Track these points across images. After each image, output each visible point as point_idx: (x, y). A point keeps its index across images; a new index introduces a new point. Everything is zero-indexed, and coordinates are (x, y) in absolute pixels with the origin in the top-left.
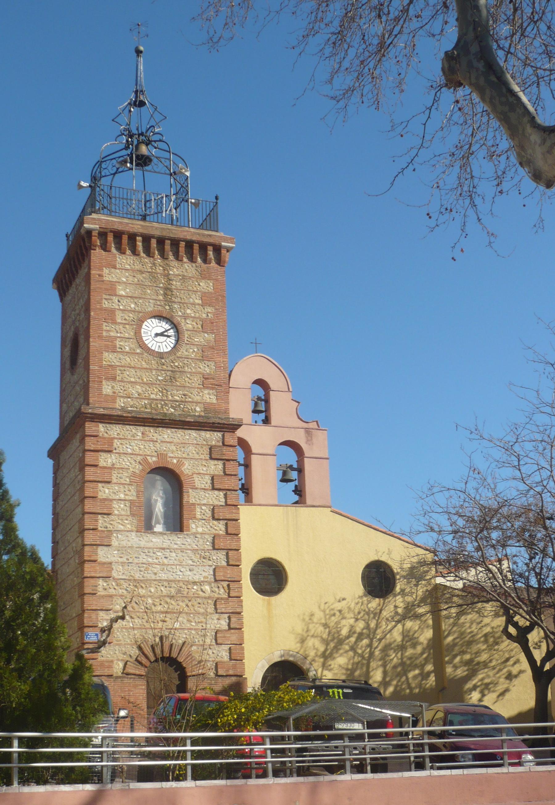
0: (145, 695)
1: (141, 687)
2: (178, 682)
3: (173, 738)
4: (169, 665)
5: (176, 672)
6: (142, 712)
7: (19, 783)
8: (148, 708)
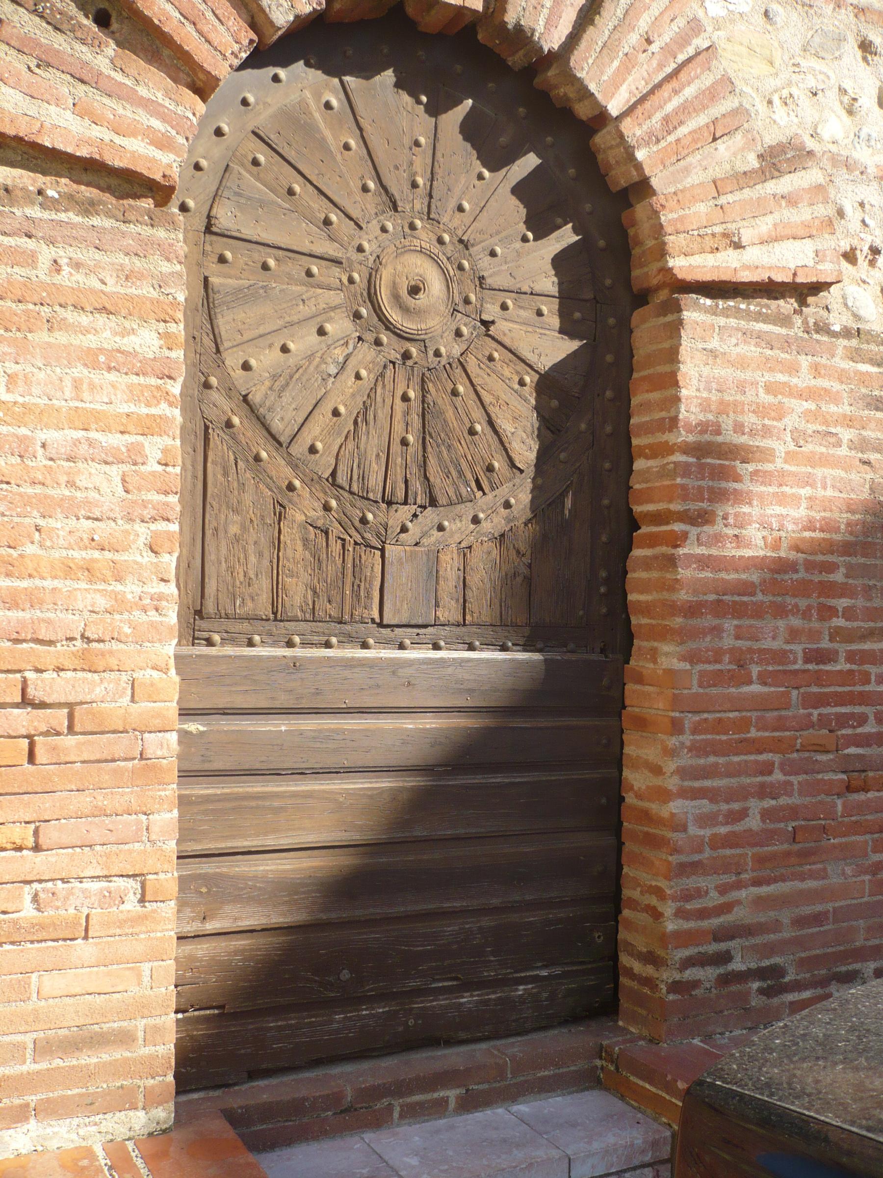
0: (163, 450)
1: (104, 333)
2: (552, 348)
3: (417, 1103)
4: (471, 130)
5: (540, 225)
6: (102, 692)
7: (89, 1153)
8: (197, 620)
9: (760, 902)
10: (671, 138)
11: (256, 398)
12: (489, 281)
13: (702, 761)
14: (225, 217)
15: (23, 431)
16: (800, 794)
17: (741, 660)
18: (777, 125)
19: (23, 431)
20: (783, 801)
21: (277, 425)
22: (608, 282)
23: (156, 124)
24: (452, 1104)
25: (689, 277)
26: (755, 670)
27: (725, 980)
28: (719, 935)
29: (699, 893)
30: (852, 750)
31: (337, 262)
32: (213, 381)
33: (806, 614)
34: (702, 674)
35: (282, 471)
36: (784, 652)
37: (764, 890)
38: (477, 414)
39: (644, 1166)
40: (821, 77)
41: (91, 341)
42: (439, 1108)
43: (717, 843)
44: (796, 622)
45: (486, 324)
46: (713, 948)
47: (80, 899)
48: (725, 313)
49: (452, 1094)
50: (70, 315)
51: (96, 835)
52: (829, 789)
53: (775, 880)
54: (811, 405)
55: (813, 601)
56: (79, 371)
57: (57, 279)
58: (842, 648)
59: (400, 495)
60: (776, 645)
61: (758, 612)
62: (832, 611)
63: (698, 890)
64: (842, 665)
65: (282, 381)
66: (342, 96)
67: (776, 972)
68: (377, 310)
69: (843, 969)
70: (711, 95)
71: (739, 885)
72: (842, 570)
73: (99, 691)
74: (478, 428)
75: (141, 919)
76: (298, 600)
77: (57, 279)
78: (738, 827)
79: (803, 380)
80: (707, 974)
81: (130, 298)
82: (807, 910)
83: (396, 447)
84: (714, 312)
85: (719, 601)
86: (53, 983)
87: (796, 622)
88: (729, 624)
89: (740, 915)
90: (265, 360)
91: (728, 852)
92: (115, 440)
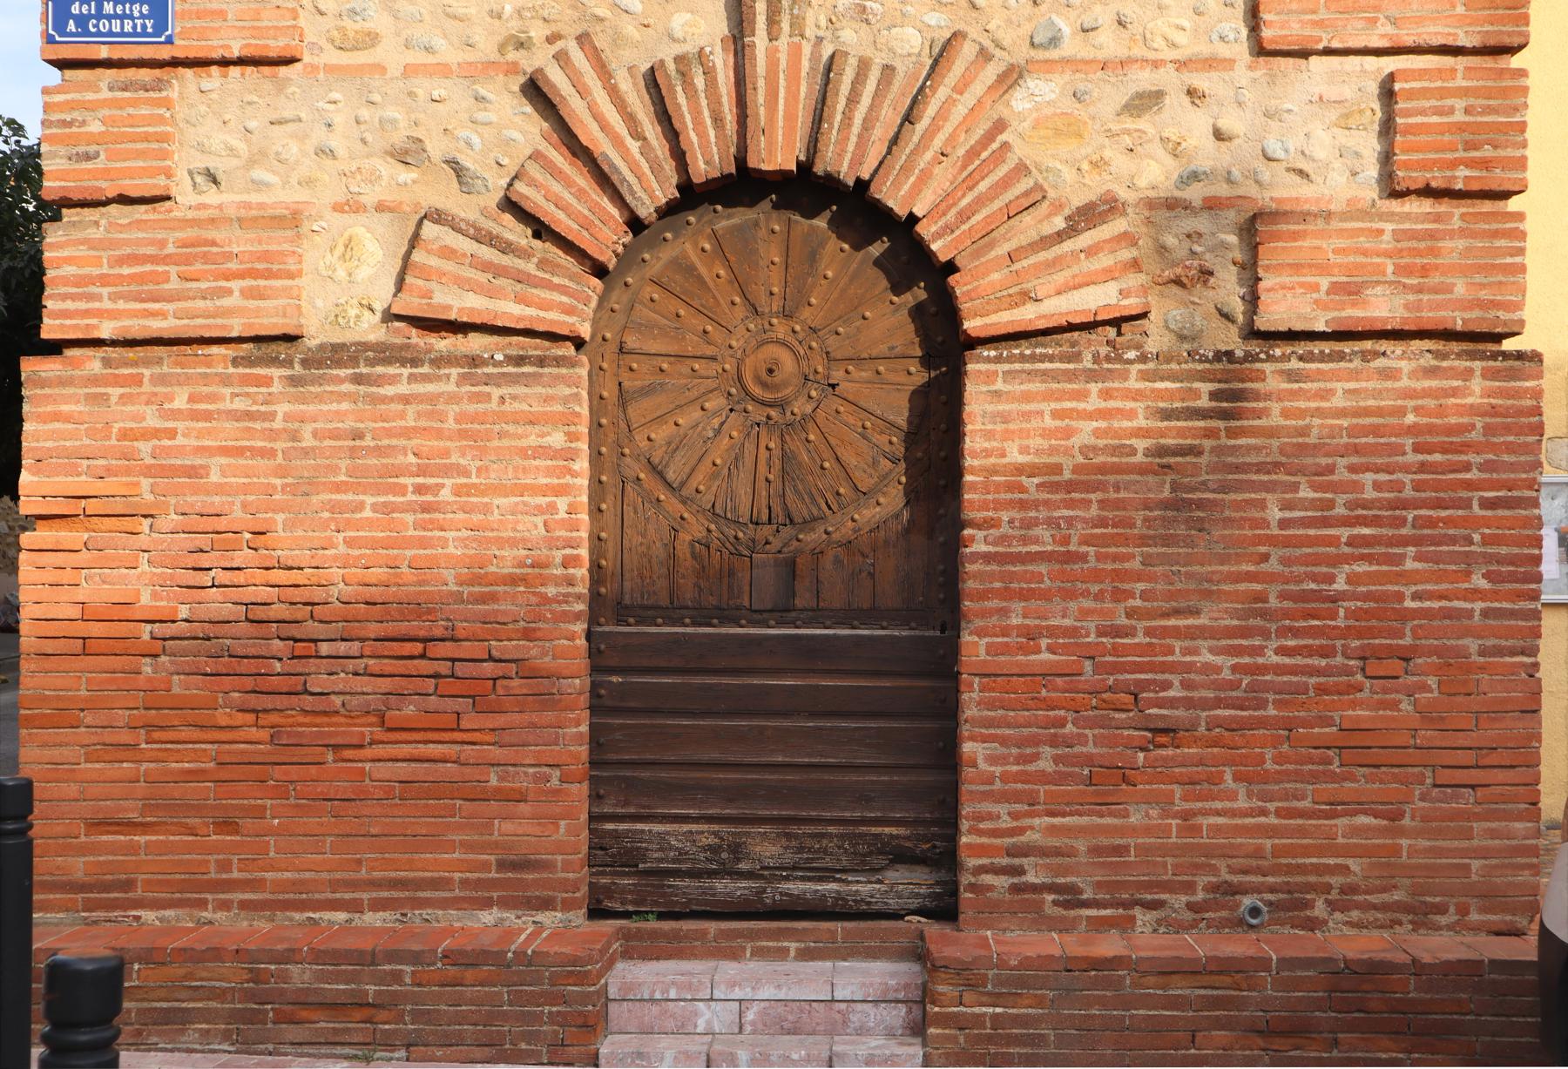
9: (1052, 830)
10: (965, 227)
11: (656, 461)
12: (832, 355)
13: (992, 714)
14: (632, 342)
15: (486, 500)
16: (1095, 744)
17: (1031, 635)
18: (1077, 190)
19: (486, 500)
20: (1078, 749)
21: (671, 475)
22: (940, 339)
23: (565, 299)
24: (792, 953)
25: (983, 334)
26: (1044, 642)
27: (1016, 889)
28: (1011, 852)
29: (990, 817)
30: (1154, 711)
31: (713, 359)
32: (627, 451)
33: (1098, 597)
34: (989, 646)
35: (673, 505)
36: (1075, 629)
37: (1057, 820)
38: (827, 454)
39: (898, 1001)
40: (1136, 135)
41: (524, 443)
42: (782, 954)
43: (1005, 778)
44: (1087, 603)
45: (833, 386)
46: (1005, 861)
47: (523, 780)
48: (1011, 359)
49: (793, 946)
50: (511, 428)
51: (531, 739)
52: (1130, 745)
53: (1071, 814)
54: (1102, 424)
55: (1107, 586)
56: (519, 461)
57: (503, 408)
58: (1140, 625)
59: (765, 518)
60: (1067, 622)
61: (1045, 596)
62: (1130, 594)
63: (990, 813)
64: (1140, 639)
65: (674, 447)
66: (714, 241)
67: (1073, 889)
68: (744, 388)
69: (1149, 897)
70: (1005, 183)
71: (1031, 815)
72: (1139, 558)
73: (534, 652)
74: (827, 465)
75: (557, 792)
76: (688, 595)
77: (503, 408)
78: (1031, 768)
79: (1094, 403)
80: (1002, 882)
81: (545, 413)
82: (1105, 841)
83: (761, 484)
84: (998, 360)
85: (1006, 589)
86: (508, 827)
87: (1087, 603)
88: (1018, 606)
89: (1030, 837)
90: (661, 434)
91: (1019, 786)
92: (542, 501)
